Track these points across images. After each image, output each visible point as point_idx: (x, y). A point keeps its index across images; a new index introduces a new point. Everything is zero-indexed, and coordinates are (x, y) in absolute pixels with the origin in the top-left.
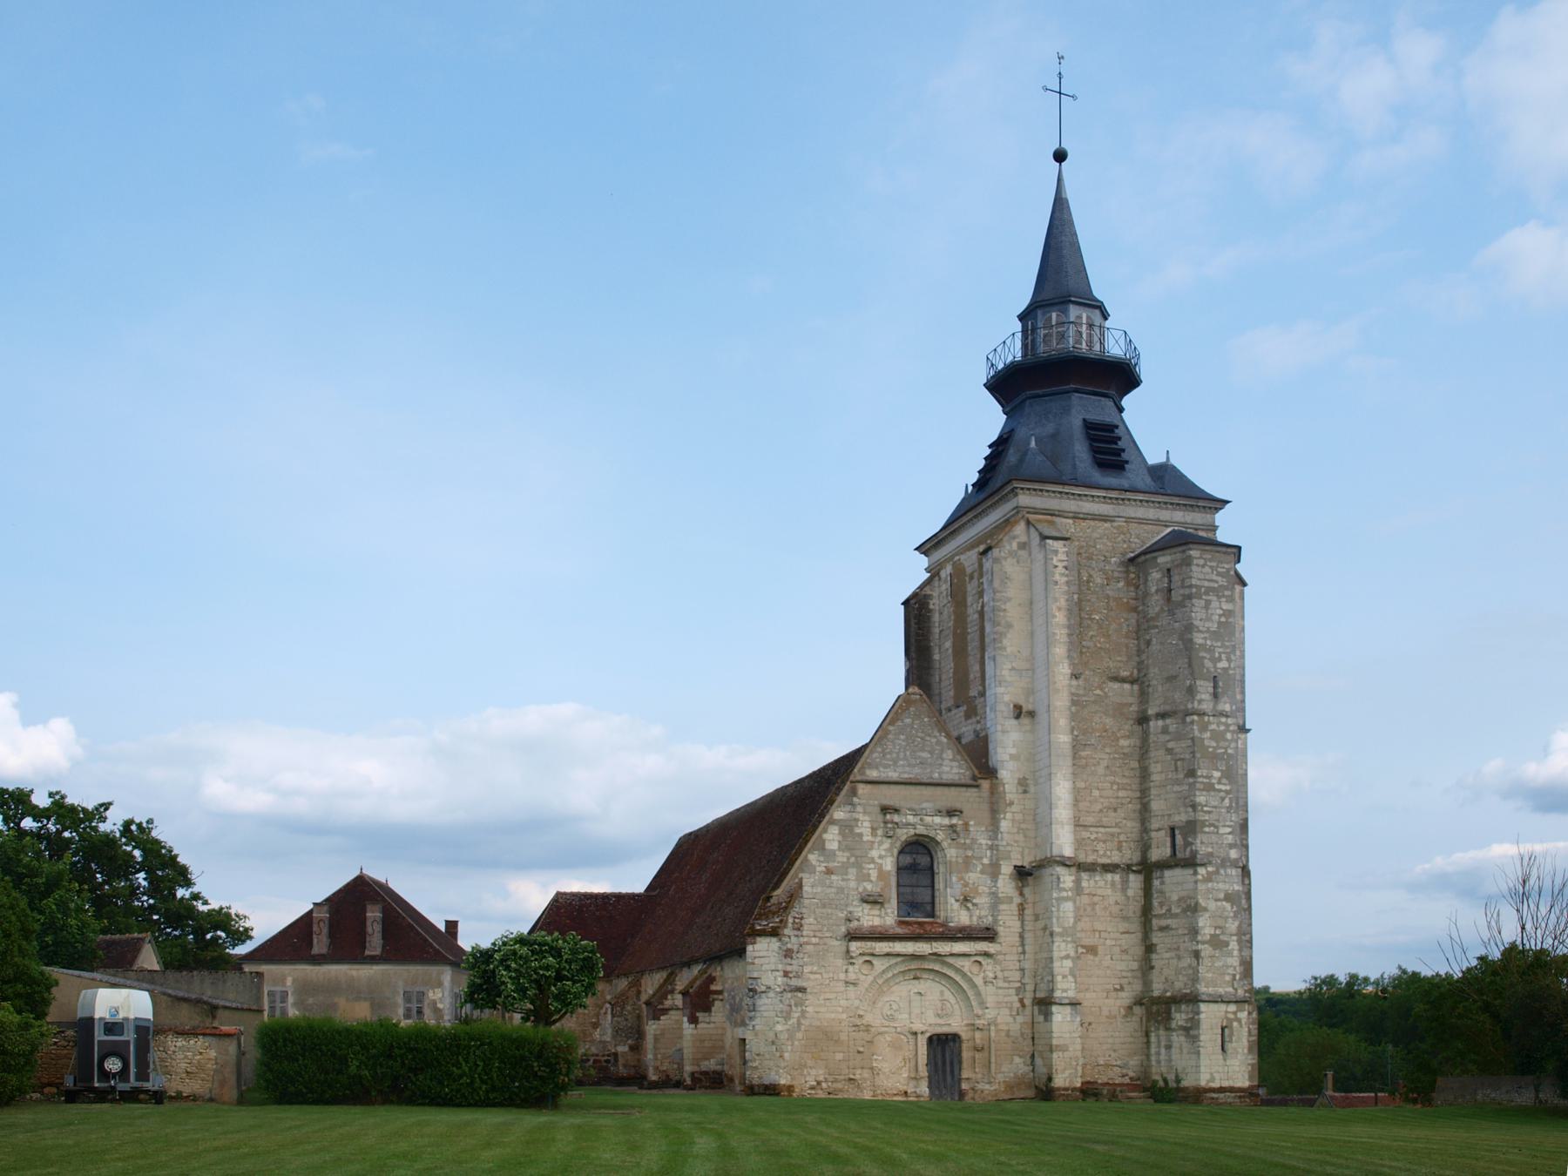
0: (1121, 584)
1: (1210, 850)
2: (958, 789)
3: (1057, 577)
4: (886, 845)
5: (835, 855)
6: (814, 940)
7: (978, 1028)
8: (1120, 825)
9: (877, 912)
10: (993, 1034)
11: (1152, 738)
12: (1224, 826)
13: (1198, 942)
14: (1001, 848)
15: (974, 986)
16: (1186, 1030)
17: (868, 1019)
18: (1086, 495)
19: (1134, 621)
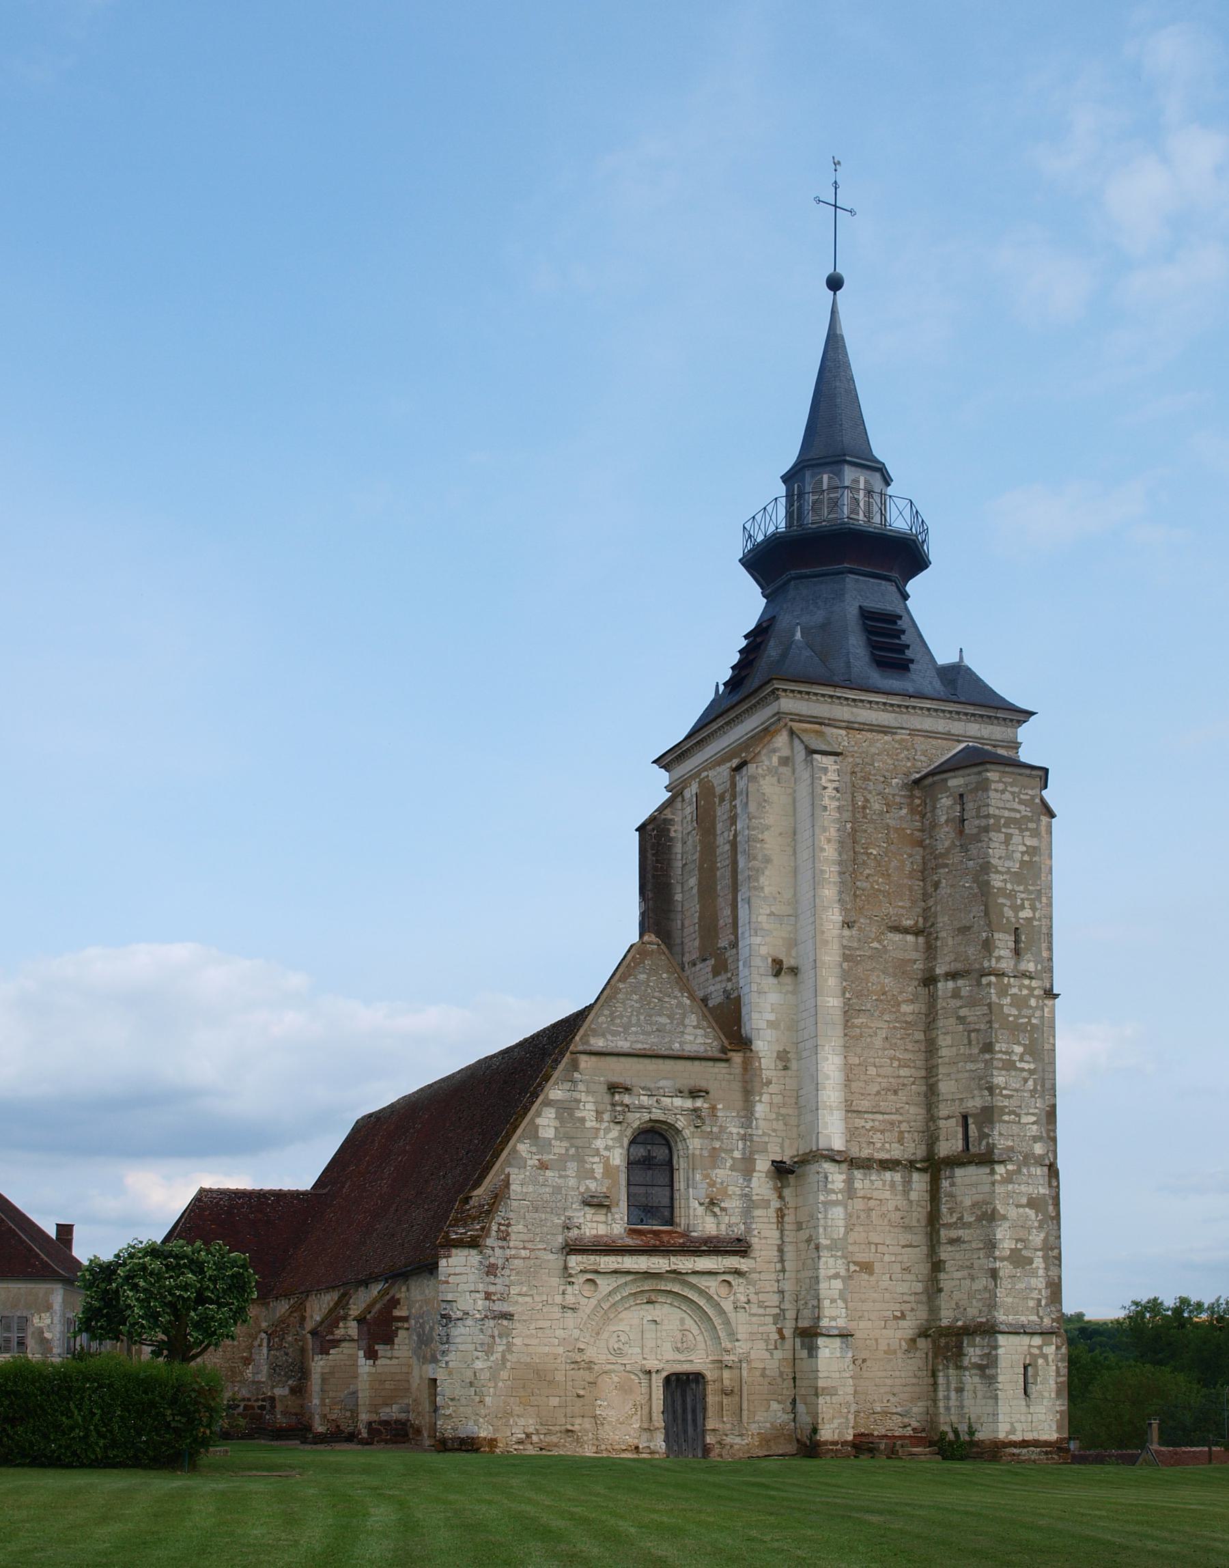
0: (904, 811)
2: (704, 1063)
3: (826, 801)
4: (614, 1133)
5: (550, 1144)
6: (524, 1253)
7: (726, 1366)
8: (901, 1111)
9: (602, 1218)
10: (745, 1373)
11: (941, 1003)
13: (995, 1258)
15: (722, 1312)
16: (981, 1368)
17: (591, 1353)
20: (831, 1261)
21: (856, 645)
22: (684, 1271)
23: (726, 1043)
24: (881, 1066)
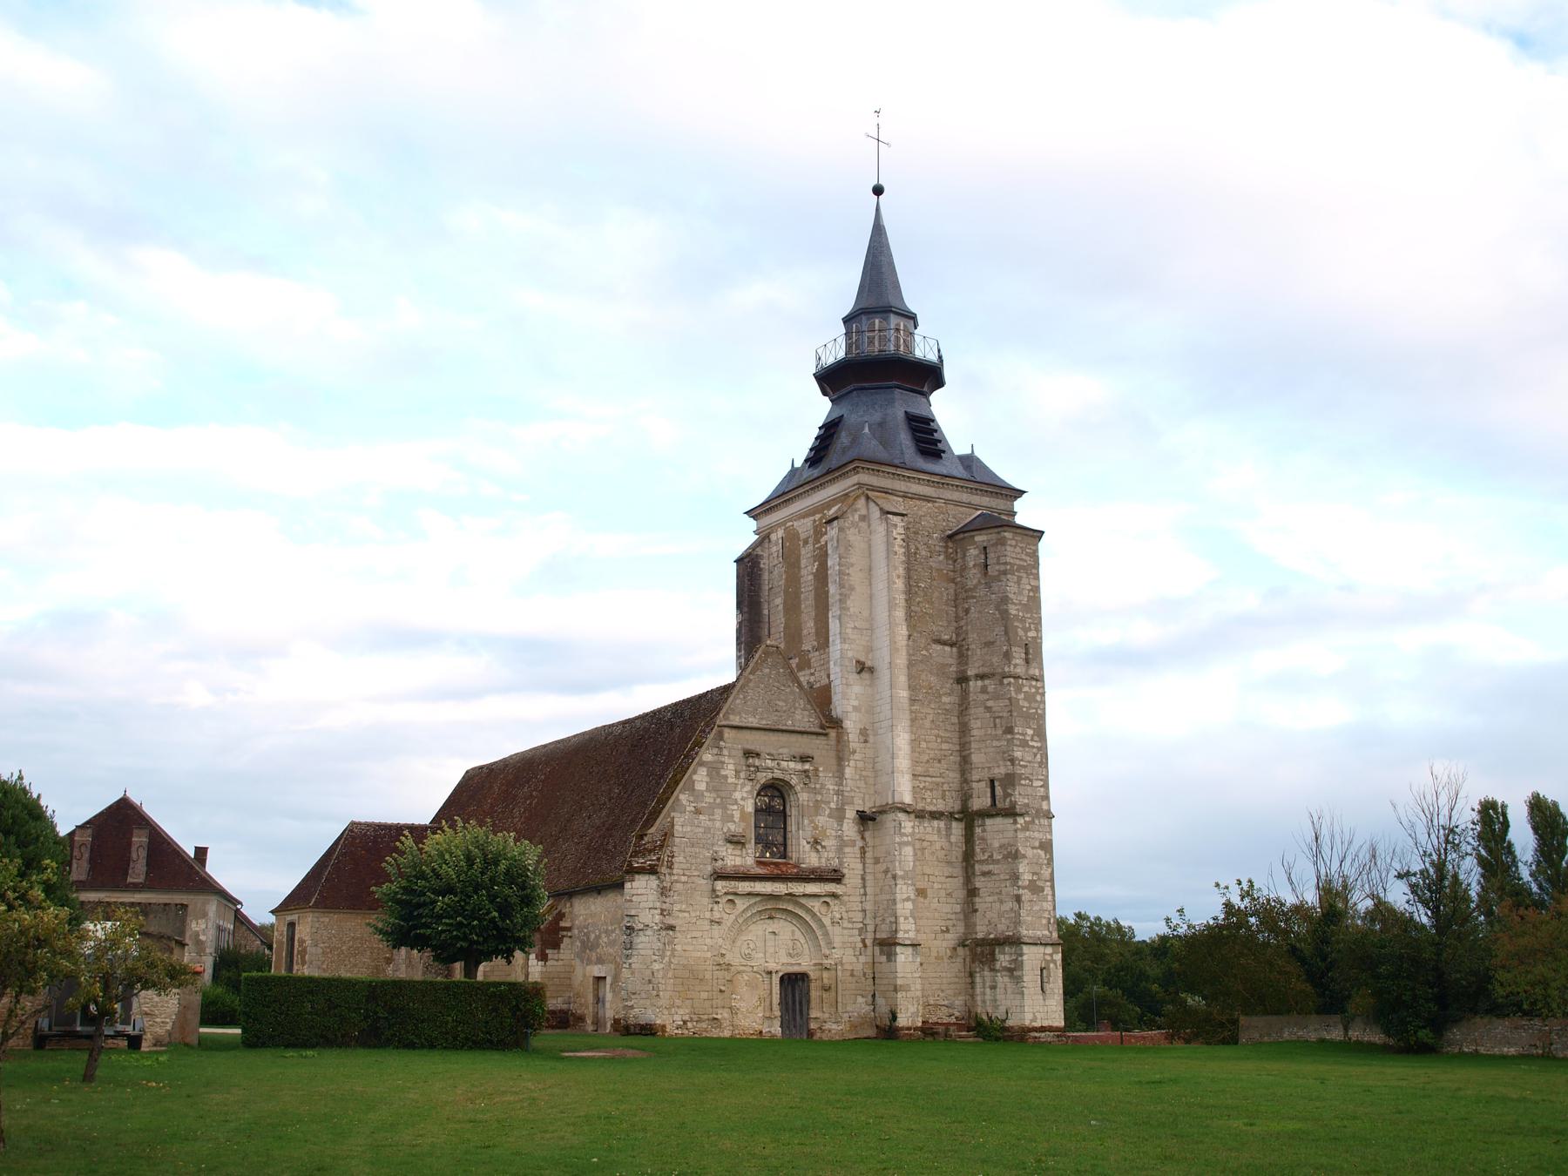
0: (941, 558)
1: (1026, 801)
2: (810, 737)
3: (897, 548)
4: (748, 788)
5: (703, 795)
6: (684, 879)
8: (944, 775)
9: (738, 852)
10: (839, 973)
11: (972, 697)
12: (1037, 780)
13: (1018, 887)
14: (846, 794)
15: (822, 926)
16: (1011, 970)
17: (729, 958)
18: (914, 478)
19: (952, 591)
20: (905, 887)
21: (905, 439)
22: (797, 894)
23: (824, 722)
24: (929, 742)
